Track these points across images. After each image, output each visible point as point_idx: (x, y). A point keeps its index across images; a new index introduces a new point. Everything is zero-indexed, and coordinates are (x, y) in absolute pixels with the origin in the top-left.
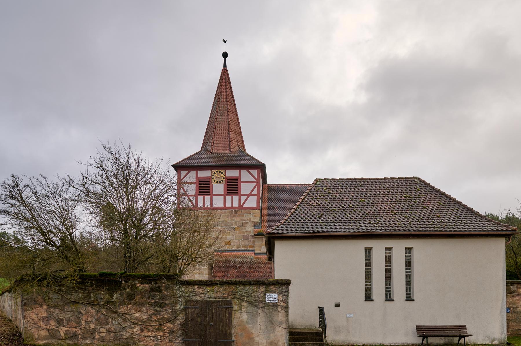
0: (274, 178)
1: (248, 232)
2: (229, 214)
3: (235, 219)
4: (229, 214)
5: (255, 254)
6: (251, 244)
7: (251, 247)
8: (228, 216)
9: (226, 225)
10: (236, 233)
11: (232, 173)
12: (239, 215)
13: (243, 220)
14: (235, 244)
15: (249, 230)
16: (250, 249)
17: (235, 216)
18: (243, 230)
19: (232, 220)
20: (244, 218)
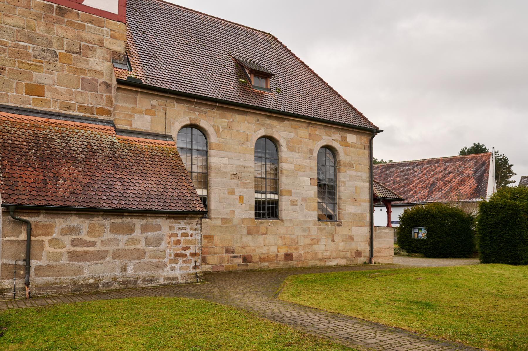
0: (383, 151)
1: (96, 72)
2: (40, 11)
3: (59, 30)
4: (40, 11)
5: (118, 131)
6: (103, 104)
7: (101, 111)
8: (38, 17)
9: (30, 39)
10: (62, 69)
11: (332, 138)
12: (70, 23)
13: (81, 39)
14: (57, 96)
15: (99, 68)
16: (101, 117)
17: (58, 22)
18: (83, 66)
19: (49, 31)
20: (84, 34)
